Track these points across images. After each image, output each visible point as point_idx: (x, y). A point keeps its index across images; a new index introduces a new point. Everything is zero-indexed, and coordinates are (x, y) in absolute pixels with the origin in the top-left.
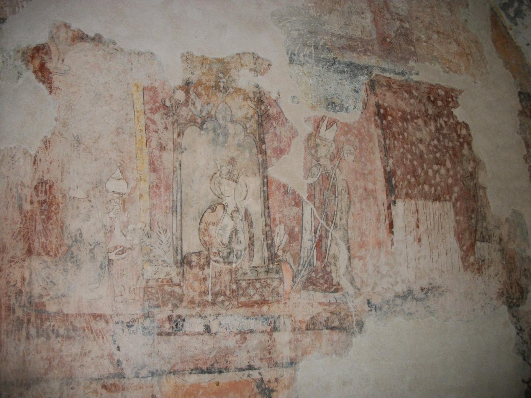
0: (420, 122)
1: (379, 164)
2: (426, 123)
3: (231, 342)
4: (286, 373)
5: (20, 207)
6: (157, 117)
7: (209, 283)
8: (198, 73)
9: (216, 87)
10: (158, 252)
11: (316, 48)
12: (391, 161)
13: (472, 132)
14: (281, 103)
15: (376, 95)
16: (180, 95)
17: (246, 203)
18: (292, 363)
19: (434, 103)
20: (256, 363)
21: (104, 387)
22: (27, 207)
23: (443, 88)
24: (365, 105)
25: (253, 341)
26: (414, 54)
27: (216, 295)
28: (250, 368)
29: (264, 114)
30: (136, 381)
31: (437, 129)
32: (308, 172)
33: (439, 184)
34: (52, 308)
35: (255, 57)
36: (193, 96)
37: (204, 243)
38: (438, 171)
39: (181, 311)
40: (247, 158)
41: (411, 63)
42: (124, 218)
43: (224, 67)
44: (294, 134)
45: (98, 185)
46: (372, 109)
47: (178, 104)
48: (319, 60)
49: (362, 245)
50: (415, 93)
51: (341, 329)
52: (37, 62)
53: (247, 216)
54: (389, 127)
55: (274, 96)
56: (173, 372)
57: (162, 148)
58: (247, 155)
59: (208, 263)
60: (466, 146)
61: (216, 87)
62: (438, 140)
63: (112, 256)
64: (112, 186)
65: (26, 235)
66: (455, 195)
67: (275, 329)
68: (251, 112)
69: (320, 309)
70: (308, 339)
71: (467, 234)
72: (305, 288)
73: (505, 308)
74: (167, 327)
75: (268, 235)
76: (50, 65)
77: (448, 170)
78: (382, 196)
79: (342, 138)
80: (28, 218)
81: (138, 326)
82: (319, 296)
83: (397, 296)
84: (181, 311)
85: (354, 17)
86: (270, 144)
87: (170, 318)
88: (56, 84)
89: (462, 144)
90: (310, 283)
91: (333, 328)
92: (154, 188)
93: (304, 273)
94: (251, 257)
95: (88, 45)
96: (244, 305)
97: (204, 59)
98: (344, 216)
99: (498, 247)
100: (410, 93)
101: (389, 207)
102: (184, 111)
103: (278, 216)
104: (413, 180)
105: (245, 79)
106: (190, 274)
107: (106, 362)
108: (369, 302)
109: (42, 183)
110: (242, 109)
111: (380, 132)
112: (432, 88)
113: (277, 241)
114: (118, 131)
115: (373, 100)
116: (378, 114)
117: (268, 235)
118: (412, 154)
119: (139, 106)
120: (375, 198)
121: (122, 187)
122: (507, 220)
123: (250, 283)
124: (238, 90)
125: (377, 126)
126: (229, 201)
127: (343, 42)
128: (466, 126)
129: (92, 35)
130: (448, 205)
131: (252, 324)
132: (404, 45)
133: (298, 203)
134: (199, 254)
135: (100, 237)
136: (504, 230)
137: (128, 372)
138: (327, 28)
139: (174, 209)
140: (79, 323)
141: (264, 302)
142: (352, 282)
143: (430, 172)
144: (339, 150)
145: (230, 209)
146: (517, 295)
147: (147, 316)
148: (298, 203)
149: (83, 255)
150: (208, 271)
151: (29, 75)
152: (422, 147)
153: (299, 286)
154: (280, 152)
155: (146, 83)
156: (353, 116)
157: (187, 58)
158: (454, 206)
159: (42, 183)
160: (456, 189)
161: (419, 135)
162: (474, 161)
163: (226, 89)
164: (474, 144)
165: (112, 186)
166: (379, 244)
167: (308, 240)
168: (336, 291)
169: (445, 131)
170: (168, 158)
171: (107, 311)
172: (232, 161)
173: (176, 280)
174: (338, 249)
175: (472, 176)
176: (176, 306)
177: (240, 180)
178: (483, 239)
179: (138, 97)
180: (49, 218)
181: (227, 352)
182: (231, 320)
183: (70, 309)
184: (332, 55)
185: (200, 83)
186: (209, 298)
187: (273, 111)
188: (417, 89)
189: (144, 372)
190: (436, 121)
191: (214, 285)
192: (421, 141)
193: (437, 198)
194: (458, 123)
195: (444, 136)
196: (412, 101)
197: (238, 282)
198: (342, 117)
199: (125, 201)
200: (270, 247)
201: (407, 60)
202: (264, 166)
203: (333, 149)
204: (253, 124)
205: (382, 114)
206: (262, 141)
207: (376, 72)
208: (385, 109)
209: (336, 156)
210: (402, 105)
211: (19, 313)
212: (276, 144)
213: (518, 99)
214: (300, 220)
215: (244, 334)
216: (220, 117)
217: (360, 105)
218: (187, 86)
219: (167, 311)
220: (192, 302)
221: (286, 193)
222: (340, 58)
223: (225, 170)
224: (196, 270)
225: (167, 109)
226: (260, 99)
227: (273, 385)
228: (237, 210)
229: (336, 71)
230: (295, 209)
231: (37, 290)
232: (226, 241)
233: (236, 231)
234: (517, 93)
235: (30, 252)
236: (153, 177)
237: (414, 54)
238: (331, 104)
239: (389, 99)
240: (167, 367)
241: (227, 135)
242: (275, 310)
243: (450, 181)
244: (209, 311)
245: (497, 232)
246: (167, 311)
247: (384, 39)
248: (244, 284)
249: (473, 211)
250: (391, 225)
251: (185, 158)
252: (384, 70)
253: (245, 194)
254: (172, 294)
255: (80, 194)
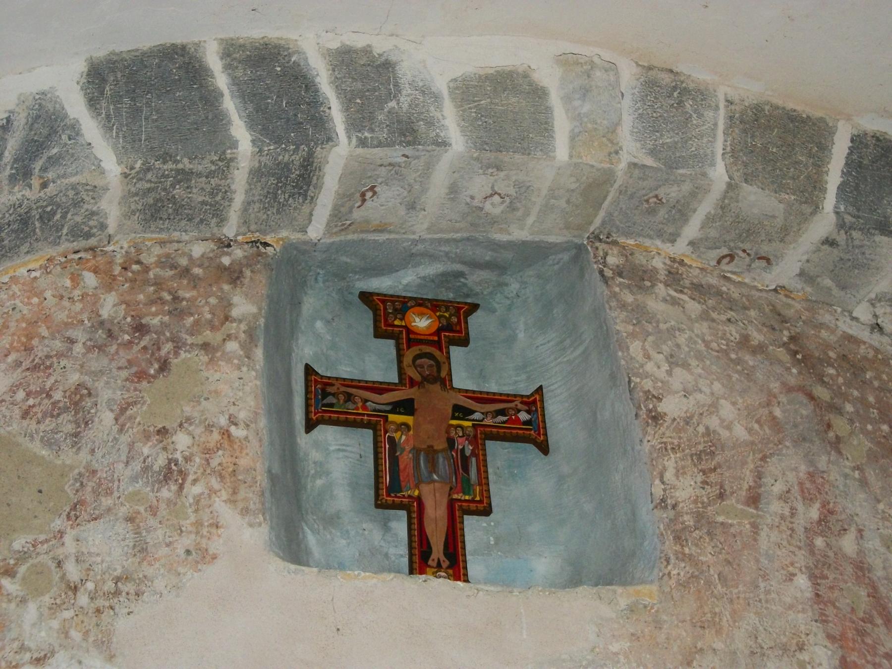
202: (874, 594)
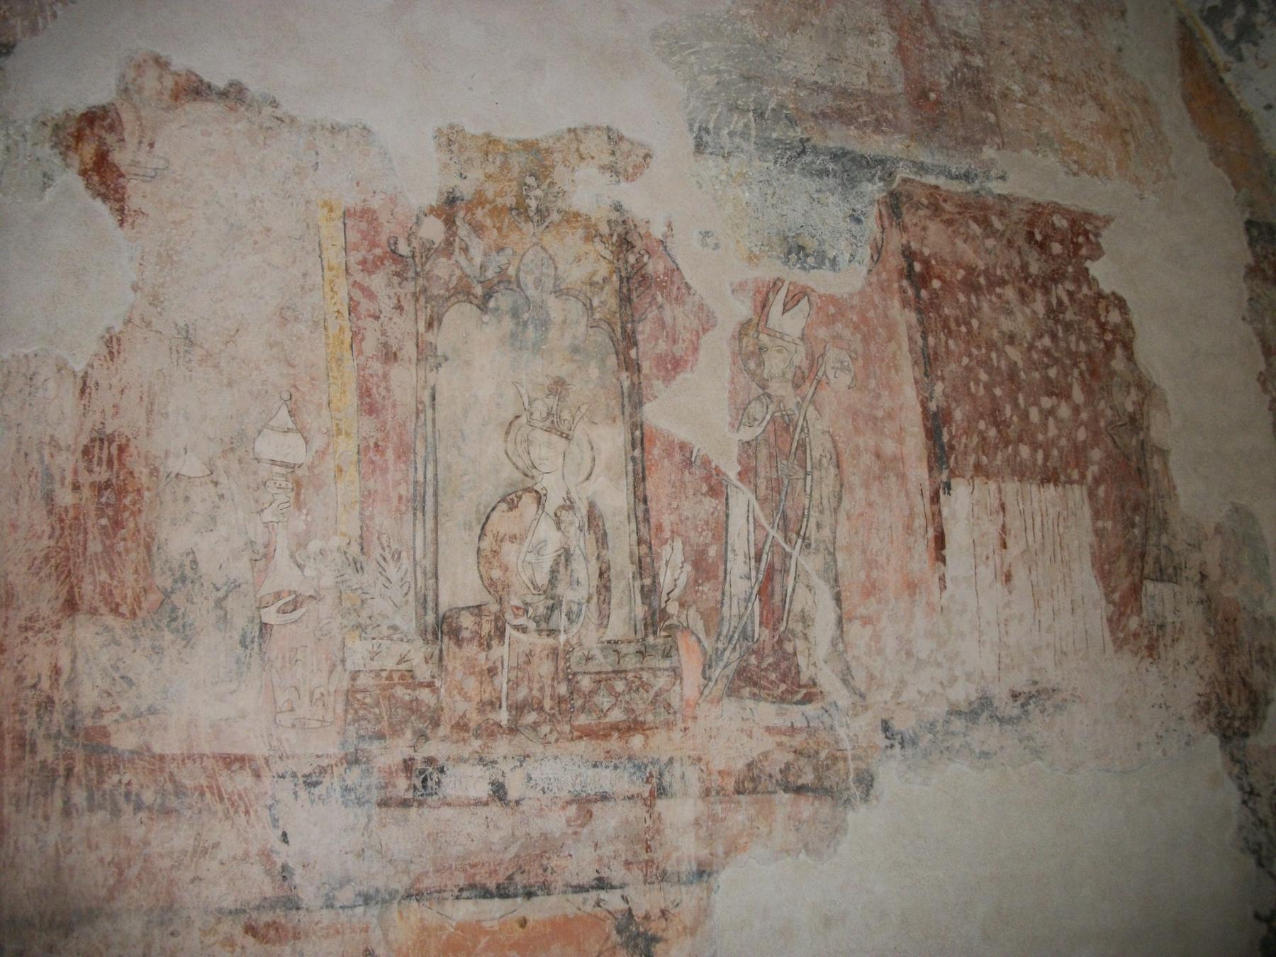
0: (1010, 293)
1: (910, 395)
2: (1023, 295)
3: (556, 822)
4: (687, 898)
5: (49, 498)
6: (377, 282)
7: (502, 681)
8: (475, 175)
9: (520, 208)
10: (380, 605)
11: (760, 115)
12: (939, 387)
13: (1135, 319)
14: (676, 248)
15: (904, 229)
16: (433, 230)
17: (591, 488)
18: (703, 872)
19: (1043, 246)
20: (616, 873)
21: (251, 930)
22: (65, 498)
23: (1065, 212)
24: (878, 252)
25: (608, 819)
26: (996, 129)
27: (519, 709)
28: (602, 884)
29: (635, 273)
30: (326, 916)
31: (1050, 311)
32: (741, 415)
33: (1054, 442)
34: (124, 740)
35: (614, 138)
36: (463, 231)
37: (490, 585)
38: (1051, 412)
39: (434, 748)
40: (593, 380)
41: (989, 152)
42: (299, 524)
43: (538, 160)
44: (707, 322)
45: (237, 445)
46: (895, 261)
47: (428, 250)
48: (765, 145)
49: (871, 589)
50: (997, 224)
51: (820, 790)
52: (89, 150)
53: (593, 518)
54: (934, 304)
55: (658, 231)
56: (415, 894)
57: (390, 356)
58: (594, 372)
59: (501, 632)
60: (1119, 351)
61: (520, 208)
62: (1054, 336)
63: (270, 616)
64: (270, 446)
65: (63, 565)
66: (1093, 470)
67: (661, 791)
68: (603, 270)
69: (769, 742)
70: (739, 815)
71: (1123, 563)
72: (732, 691)
73: (1213, 740)
74: (402, 785)
75: (644, 566)
76: (120, 157)
77: (1076, 410)
78: (918, 472)
79: (822, 333)
80: (67, 524)
81: (331, 783)
82: (767, 712)
83: (955, 712)
84: (434, 748)
85: (851, 42)
86: (649, 347)
87: (408, 765)
88: (134, 202)
89: (1109, 347)
90: (745, 680)
91: (800, 790)
92: (371, 452)
93: (732, 657)
94: (604, 618)
95: (211, 109)
96: (587, 733)
97: (491, 141)
98: (827, 519)
99: (1197, 594)
100: (985, 223)
101: (935, 499)
102: (442, 268)
103: (667, 520)
104: (992, 432)
105: (588, 190)
106: (457, 658)
107: (256, 871)
108: (886, 727)
109: (102, 439)
110: (582, 262)
111: (913, 317)
112: (1038, 213)
113: (666, 580)
114: (285, 316)
115: (896, 240)
116: (909, 274)
117: (644, 566)
118: (990, 370)
119: (334, 256)
120: (902, 477)
121: (294, 449)
122: (1218, 530)
123: (602, 680)
124: (572, 218)
125: (905, 304)
126: (551, 484)
127: (825, 101)
128: (1121, 304)
129: (220, 83)
130: (1077, 494)
131: (606, 779)
132: (970, 108)
133: (716, 488)
134: (478, 610)
135: (241, 569)
136: (1212, 554)
137: (308, 894)
138: (787, 67)
139: (417, 503)
140: (190, 777)
141: (634, 726)
142: (846, 678)
143: (1034, 415)
144: (814, 361)
145: (553, 502)
146: (1243, 709)
147: (353, 760)
148: (716, 488)
149: (200, 612)
150: (500, 651)
151: (70, 179)
152: (1014, 353)
153: (719, 688)
154: (673, 366)
155: (352, 200)
156: (848, 278)
157: (450, 139)
158: (1092, 495)
159: (102, 439)
160: (1096, 454)
161: (1007, 325)
162: (1140, 387)
163: (542, 213)
164: (1140, 347)
165: (270, 446)
166: (912, 587)
167: (740, 576)
168: (808, 699)
169: (1069, 316)
170: (403, 381)
171: (258, 748)
172: (558, 387)
173: (424, 672)
174: (812, 599)
175: (1135, 422)
176: (422, 736)
177: (578, 433)
178: (1161, 576)
179: (332, 232)
180: (117, 524)
181: (546, 847)
182: (556, 769)
183: (168, 743)
184: (797, 133)
185: (480, 200)
186: (503, 716)
187: (655, 267)
188: (1002, 214)
189: (346, 896)
190: (1047, 291)
191: (514, 685)
192: (1011, 339)
193: (1050, 477)
194: (1100, 295)
195: (1068, 326)
196: (990, 243)
197: (571, 678)
198: (822, 281)
199: (299, 483)
200: (648, 593)
201: (977, 145)
202: (634, 399)
203: (800, 358)
204: (607, 299)
205: (917, 274)
206: (630, 339)
207: (903, 172)
208: (926, 263)
209: (807, 376)
210: (966, 251)
211: (46, 752)
212: (662, 346)
213: (1245, 239)
214: (721, 530)
215: (585, 804)
216: (528, 280)
217: (866, 253)
218: (449, 207)
219: (401, 748)
220: (461, 726)
221: (688, 463)
222: (817, 140)
223: (540, 409)
224: (471, 650)
225: (401, 262)
226: (624, 239)
227: (655, 927)
228: (569, 506)
229: (808, 171)
230: (710, 503)
231: (89, 698)
232: (542, 579)
233: (566, 555)
234: (1241, 225)
235: (71, 605)
236: (368, 425)
237: (996, 129)
238: (796, 250)
239: (934, 239)
240: (401, 883)
241: (544, 324)
242: (661, 745)
243: (1082, 435)
244: (502, 747)
245: (1195, 558)
246: (401, 748)
247: (924, 95)
248: (586, 683)
249: (1136, 508)
250: (940, 541)
251: (445, 379)
252: (922, 168)
253: (588, 468)
254: (413, 708)
255: (192, 466)
